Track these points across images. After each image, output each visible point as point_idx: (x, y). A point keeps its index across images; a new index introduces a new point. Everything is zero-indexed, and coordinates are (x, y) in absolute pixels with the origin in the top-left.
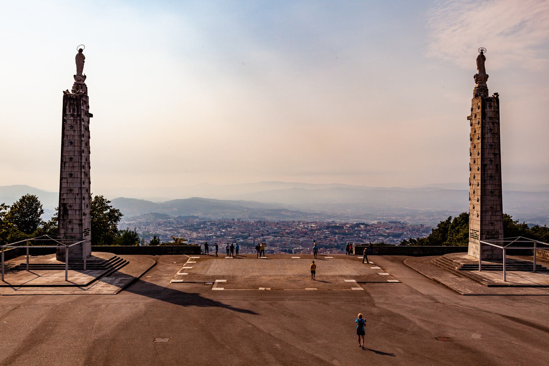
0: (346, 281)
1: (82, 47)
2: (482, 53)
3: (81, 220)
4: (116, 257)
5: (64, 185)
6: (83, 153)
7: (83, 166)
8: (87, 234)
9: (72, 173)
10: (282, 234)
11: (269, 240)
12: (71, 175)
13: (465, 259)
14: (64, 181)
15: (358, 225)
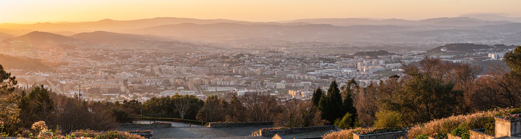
15: (242, 55)
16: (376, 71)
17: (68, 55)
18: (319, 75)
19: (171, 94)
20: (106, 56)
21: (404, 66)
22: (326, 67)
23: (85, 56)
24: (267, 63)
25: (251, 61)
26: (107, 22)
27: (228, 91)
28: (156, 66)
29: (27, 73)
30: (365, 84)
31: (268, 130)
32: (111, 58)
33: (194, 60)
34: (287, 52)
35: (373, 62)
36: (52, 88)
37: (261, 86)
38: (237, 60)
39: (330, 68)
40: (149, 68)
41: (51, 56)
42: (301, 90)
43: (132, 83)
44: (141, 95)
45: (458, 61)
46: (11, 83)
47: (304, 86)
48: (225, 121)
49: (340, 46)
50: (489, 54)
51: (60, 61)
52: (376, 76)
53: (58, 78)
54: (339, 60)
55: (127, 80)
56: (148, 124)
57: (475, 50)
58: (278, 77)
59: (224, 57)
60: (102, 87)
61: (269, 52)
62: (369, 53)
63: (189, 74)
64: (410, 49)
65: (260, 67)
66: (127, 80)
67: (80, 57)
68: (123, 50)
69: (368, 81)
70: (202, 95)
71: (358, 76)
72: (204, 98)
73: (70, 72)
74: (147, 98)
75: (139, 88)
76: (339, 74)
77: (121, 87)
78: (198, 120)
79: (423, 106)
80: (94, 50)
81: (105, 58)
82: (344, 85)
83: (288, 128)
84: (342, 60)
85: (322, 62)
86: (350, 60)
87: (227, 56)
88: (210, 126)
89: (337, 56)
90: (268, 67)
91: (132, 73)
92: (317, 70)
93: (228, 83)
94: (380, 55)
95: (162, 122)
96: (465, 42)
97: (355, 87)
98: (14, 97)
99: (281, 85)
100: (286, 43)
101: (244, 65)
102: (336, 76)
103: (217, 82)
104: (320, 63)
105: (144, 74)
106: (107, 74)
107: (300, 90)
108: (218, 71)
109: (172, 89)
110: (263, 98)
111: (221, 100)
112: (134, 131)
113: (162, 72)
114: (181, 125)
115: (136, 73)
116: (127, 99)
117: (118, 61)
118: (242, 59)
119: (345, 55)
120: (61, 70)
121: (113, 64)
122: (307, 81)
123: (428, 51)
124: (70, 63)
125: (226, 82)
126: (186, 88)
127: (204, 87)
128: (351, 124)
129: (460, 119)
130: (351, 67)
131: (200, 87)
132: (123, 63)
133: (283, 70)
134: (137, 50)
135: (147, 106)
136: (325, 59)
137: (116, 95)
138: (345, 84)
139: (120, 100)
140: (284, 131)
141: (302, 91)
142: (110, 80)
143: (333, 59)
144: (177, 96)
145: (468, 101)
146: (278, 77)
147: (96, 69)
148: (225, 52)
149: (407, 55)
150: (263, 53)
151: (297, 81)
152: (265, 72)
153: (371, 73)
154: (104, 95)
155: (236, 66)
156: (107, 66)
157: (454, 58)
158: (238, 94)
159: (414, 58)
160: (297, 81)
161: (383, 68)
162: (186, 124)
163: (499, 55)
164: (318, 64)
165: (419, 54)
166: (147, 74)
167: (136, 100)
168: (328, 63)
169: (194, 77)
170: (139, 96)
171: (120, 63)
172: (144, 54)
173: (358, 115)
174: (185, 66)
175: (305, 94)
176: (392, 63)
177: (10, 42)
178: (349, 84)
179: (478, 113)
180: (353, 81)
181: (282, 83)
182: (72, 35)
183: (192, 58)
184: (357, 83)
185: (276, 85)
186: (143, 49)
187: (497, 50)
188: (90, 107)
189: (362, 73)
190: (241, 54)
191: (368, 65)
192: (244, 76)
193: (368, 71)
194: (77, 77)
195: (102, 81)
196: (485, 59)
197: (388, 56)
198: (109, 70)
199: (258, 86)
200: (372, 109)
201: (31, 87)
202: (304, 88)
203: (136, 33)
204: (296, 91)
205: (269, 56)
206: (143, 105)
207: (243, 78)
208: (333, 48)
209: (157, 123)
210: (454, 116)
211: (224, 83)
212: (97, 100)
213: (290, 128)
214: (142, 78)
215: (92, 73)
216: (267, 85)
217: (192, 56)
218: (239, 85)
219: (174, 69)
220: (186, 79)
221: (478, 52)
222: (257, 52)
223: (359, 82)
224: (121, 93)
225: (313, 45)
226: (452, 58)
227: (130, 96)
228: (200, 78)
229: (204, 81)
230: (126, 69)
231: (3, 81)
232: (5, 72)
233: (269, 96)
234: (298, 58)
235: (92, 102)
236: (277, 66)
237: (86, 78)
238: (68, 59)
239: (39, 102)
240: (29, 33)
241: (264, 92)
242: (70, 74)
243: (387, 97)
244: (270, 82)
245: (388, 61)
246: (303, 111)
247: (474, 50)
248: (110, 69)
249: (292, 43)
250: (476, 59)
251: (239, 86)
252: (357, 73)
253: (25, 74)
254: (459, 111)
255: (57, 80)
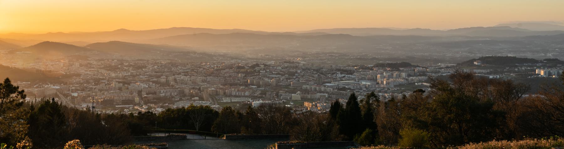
15: (257, 65)
16: (397, 84)
17: (81, 65)
18: (336, 87)
19: (186, 104)
20: (121, 67)
21: (430, 80)
22: (344, 79)
23: (99, 67)
24: (283, 73)
25: (266, 72)
26: (123, 32)
27: (243, 102)
28: (171, 76)
29: (36, 86)
30: (385, 97)
31: (284, 143)
32: (126, 69)
33: (209, 70)
34: (303, 63)
35: (395, 75)
36: (62, 101)
37: (276, 97)
38: (253, 71)
39: (347, 79)
40: (164, 78)
41: (62, 67)
42: (317, 102)
43: (147, 94)
44: (156, 106)
45: (495, 76)
46: (19, 97)
47: (320, 98)
48: (240, 133)
49: (358, 57)
50: (537, 70)
51: (72, 73)
52: (397, 89)
53: (69, 91)
54: (357, 72)
55: (142, 91)
56: (163, 137)
57: (518, 64)
58: (293, 87)
59: (239, 67)
60: (116, 98)
61: (285, 62)
62: (389, 65)
63: (204, 84)
64: (437, 61)
65: (275, 77)
66: (142, 91)
67: (93, 68)
68: (138, 60)
69: (388, 95)
70: (217, 106)
71: (378, 89)
72: (219, 108)
73: (82, 83)
74: (161, 109)
75: (154, 99)
76: (357, 86)
77: (135, 98)
78: (213, 132)
79: (455, 126)
80: (108, 61)
81: (119, 68)
82: (363, 99)
83: (305, 142)
84: (361, 72)
85: (339, 73)
86: (369, 71)
87: (242, 66)
88: (225, 138)
89: (355, 68)
90: (283, 77)
91: (147, 83)
92: (334, 82)
93: (243, 93)
94: (402, 67)
95: (177, 134)
96: (504, 55)
97: (375, 100)
98: (22, 112)
99: (297, 96)
100: (302, 53)
101: (259, 75)
102: (354, 88)
103: (232, 93)
104: (338, 74)
105: (159, 85)
106: (121, 84)
107: (316, 102)
108: (233, 81)
109: (187, 100)
110: (279, 109)
111: (236, 111)
112: (149, 144)
113: (177, 83)
114: (196, 137)
115: (151, 83)
116: (141, 111)
117: (133, 71)
118: (257, 69)
119: (364, 67)
120: (72, 81)
121: (128, 74)
122: (323, 92)
123: (458, 64)
124: (83, 74)
125: (241, 93)
126: (201, 99)
127: (219, 97)
128: (371, 141)
129: (504, 145)
130: (369, 80)
131: (215, 98)
132: (138, 73)
133: (298, 81)
134: (152, 60)
135: (162, 118)
136: (343, 70)
137: (130, 106)
138: (363, 97)
139: (134, 112)
140: (300, 145)
141: (317, 103)
142: (124, 91)
143: (351, 71)
144: (192, 106)
145: (512, 125)
146: (293, 87)
147: (110, 80)
148: (240, 62)
149: (433, 68)
150: (278, 63)
151: (313, 93)
152: (281, 82)
153: (392, 87)
154: (118, 107)
155: (251, 76)
156: (121, 77)
157: (490, 73)
158: (253, 104)
159: (441, 72)
160: (313, 93)
161: (406, 82)
162: (201, 136)
163: (551, 71)
164: (335, 75)
165: (447, 67)
166: (163, 85)
167: (150, 111)
168: (346, 74)
169: (209, 87)
170: (154, 107)
171: (135, 74)
172: (159, 64)
173: (379, 131)
174: (200, 76)
175: (322, 106)
176: (416, 76)
177: (18, 53)
178: (369, 97)
179: (528, 141)
180: (373, 94)
181: (297, 94)
182: (85, 45)
183: (208, 68)
184: (377, 97)
185: (292, 96)
186: (158, 59)
187: (548, 65)
188: (104, 119)
189: (382, 86)
190: (256, 64)
191: (391, 76)
192: (259, 86)
193: (389, 84)
194: (89, 89)
195: (116, 92)
196: (532, 75)
197: (411, 68)
199: (273, 96)
200: (394, 126)
201: (39, 101)
202: (320, 100)
203: (152, 43)
204: (312, 103)
205: (284, 66)
206: (158, 117)
207: (258, 89)
208: (351, 59)
209: (172, 135)
210: (496, 141)
211: (239, 93)
212: (110, 112)
213: (306, 142)
214: (157, 88)
215: (106, 84)
216: (282, 96)
217: (207, 66)
218: (254, 96)
219: (189, 79)
220: (201, 89)
221: (521, 67)
222: (273, 62)
223: (379, 96)
224: (135, 105)
225: (330, 56)
226: (488, 73)
227: (144, 107)
228: (215, 88)
229: (219, 91)
230: (141, 79)
231: (9, 95)
232: (12, 85)
233: (285, 107)
234: (314, 68)
235: (106, 114)
236: (293, 76)
237: (99, 90)
238: (80, 70)
239: (49, 116)
240: (39, 43)
241: (279, 103)
242: (82, 85)
243: (413, 113)
244: (286, 93)
245: (411, 74)
246: (320, 124)
247: (516, 64)
248: (125, 80)
249: (308, 53)
250: (519, 75)
251: (254, 96)
252: (377, 86)
253: (33, 87)
254: (499, 136)
255: (68, 92)
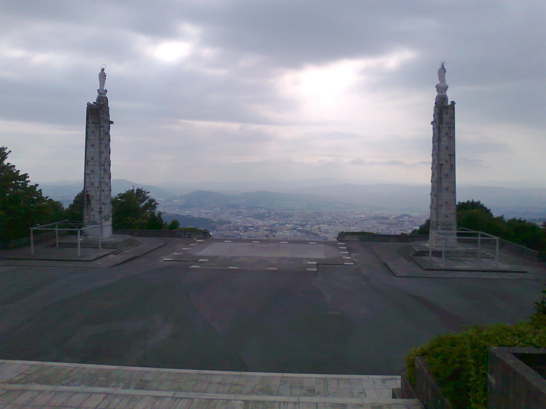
0: (309, 263)
1: (104, 67)
2: (443, 66)
3: (101, 208)
4: (132, 238)
5: (87, 180)
6: (103, 153)
7: (103, 165)
8: (107, 220)
9: (94, 170)
10: (335, 223)
11: (323, 228)
12: (92, 171)
13: (424, 246)
14: (87, 176)
15: (402, 217)
24: (18, 182)
198: (271, 229)
